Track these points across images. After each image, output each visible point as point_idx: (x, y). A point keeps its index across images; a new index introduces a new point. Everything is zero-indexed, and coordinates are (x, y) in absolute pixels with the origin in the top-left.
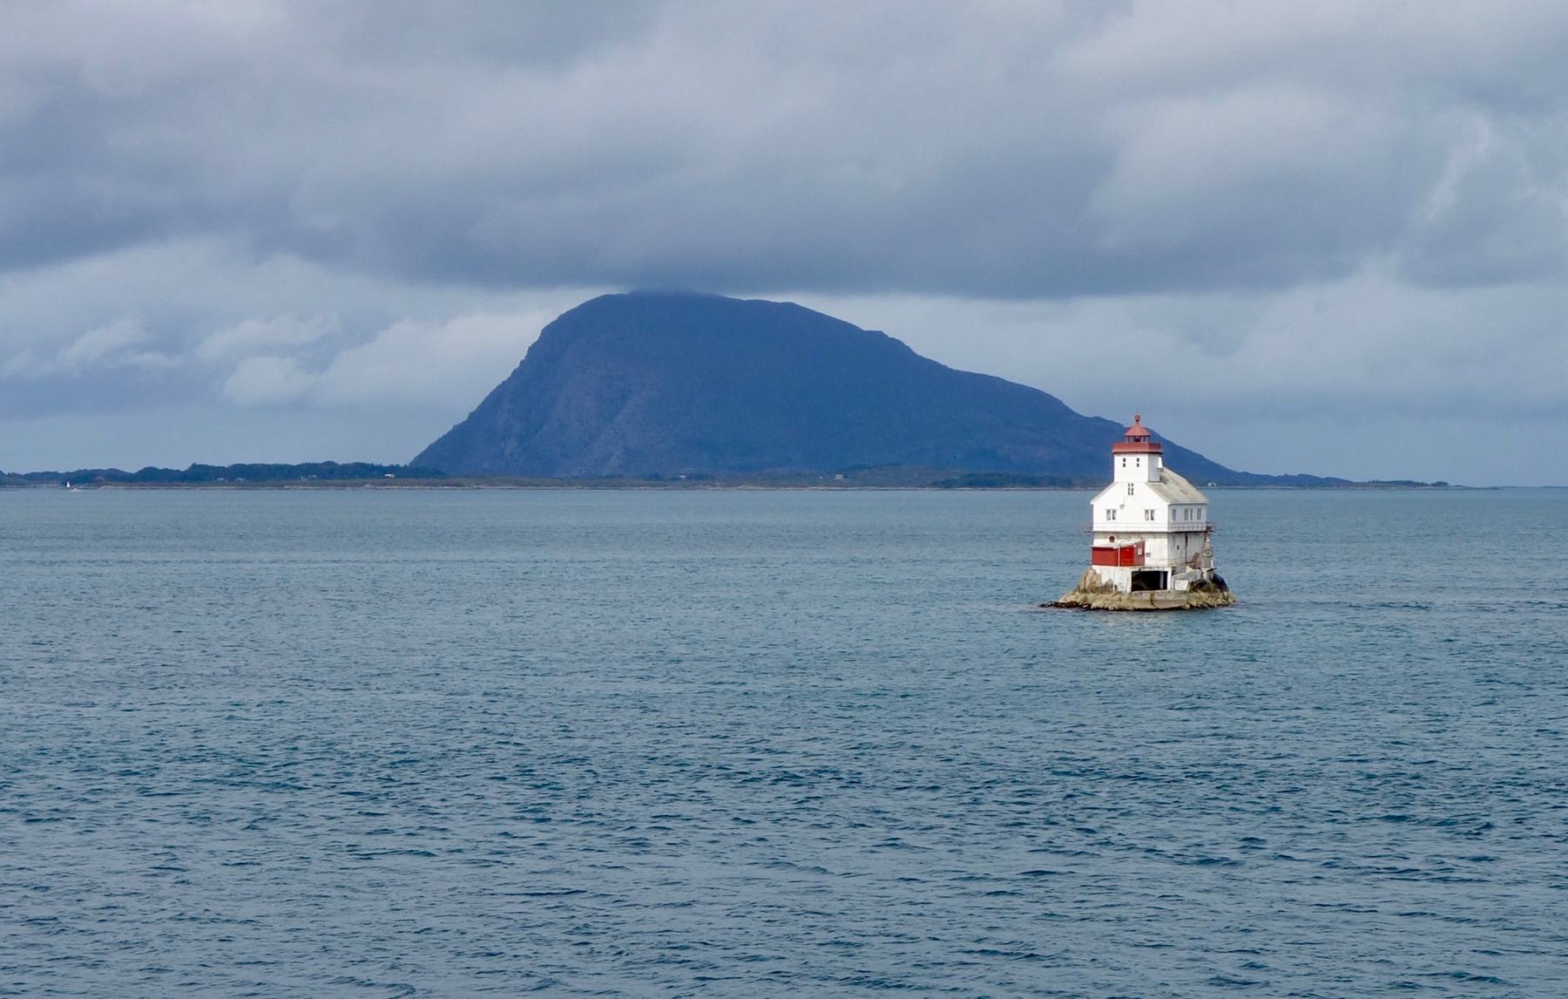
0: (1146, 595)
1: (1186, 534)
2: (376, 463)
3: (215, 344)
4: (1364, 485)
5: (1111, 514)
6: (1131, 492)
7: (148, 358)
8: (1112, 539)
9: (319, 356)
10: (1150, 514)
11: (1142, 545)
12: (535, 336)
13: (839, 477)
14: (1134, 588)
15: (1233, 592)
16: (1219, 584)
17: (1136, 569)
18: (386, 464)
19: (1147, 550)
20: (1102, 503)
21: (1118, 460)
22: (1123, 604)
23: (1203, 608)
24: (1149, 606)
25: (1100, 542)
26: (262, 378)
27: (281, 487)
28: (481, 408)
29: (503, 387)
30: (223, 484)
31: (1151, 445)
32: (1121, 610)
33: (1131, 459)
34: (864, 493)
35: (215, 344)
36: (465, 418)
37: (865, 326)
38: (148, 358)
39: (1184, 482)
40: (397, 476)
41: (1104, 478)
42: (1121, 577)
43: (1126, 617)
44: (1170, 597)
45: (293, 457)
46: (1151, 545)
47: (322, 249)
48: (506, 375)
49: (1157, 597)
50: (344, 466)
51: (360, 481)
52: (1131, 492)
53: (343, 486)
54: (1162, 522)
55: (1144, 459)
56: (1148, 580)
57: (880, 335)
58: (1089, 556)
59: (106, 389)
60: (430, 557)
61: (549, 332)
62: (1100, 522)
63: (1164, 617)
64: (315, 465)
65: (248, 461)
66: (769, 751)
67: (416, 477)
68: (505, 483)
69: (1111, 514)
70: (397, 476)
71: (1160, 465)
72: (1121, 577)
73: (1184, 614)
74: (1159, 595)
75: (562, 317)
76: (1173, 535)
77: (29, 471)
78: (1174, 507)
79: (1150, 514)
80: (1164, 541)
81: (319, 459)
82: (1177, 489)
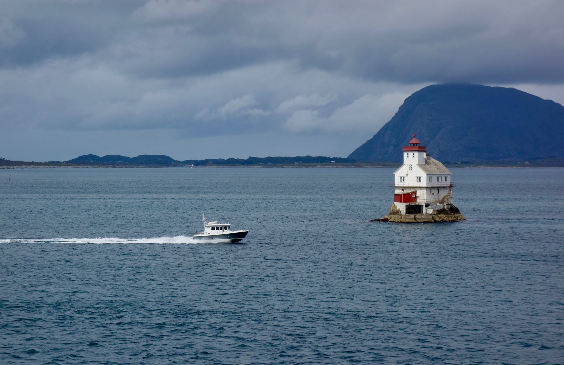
0: (412, 216)
1: (438, 188)
3: (284, 106)
4: (187, 163)
7: (255, 112)
8: (403, 190)
9: (327, 111)
10: (419, 179)
11: (415, 193)
12: (402, 103)
13: (527, 162)
14: (406, 213)
15: (463, 214)
16: (454, 210)
17: (408, 204)
18: (331, 157)
19: (417, 196)
20: (398, 174)
21: (405, 154)
22: (402, 220)
23: (443, 222)
24: (414, 221)
25: (398, 192)
26: (302, 120)
27: (282, 166)
28: (379, 133)
29: (388, 124)
30: (261, 165)
31: (419, 147)
32: (401, 222)
33: (411, 154)
35: (284, 106)
36: (372, 137)
37: (545, 98)
38: (255, 112)
39: (440, 164)
41: (399, 163)
42: (401, 207)
44: (424, 217)
45: (293, 154)
46: (419, 193)
47: (329, 65)
48: (389, 119)
49: (417, 217)
51: (316, 164)
53: (309, 166)
54: (424, 182)
55: (416, 154)
56: (417, 209)
57: (550, 102)
58: (393, 197)
59: (237, 125)
60: (168, 197)
61: (407, 101)
62: (398, 182)
63: (423, 227)
64: (301, 157)
65: (273, 156)
66: (338, 279)
68: (379, 165)
69: (402, 179)
71: (425, 156)
72: (401, 207)
73: (430, 224)
74: (418, 216)
75: (413, 94)
76: (429, 188)
78: (430, 176)
79: (419, 179)
81: (304, 155)
82: (434, 167)
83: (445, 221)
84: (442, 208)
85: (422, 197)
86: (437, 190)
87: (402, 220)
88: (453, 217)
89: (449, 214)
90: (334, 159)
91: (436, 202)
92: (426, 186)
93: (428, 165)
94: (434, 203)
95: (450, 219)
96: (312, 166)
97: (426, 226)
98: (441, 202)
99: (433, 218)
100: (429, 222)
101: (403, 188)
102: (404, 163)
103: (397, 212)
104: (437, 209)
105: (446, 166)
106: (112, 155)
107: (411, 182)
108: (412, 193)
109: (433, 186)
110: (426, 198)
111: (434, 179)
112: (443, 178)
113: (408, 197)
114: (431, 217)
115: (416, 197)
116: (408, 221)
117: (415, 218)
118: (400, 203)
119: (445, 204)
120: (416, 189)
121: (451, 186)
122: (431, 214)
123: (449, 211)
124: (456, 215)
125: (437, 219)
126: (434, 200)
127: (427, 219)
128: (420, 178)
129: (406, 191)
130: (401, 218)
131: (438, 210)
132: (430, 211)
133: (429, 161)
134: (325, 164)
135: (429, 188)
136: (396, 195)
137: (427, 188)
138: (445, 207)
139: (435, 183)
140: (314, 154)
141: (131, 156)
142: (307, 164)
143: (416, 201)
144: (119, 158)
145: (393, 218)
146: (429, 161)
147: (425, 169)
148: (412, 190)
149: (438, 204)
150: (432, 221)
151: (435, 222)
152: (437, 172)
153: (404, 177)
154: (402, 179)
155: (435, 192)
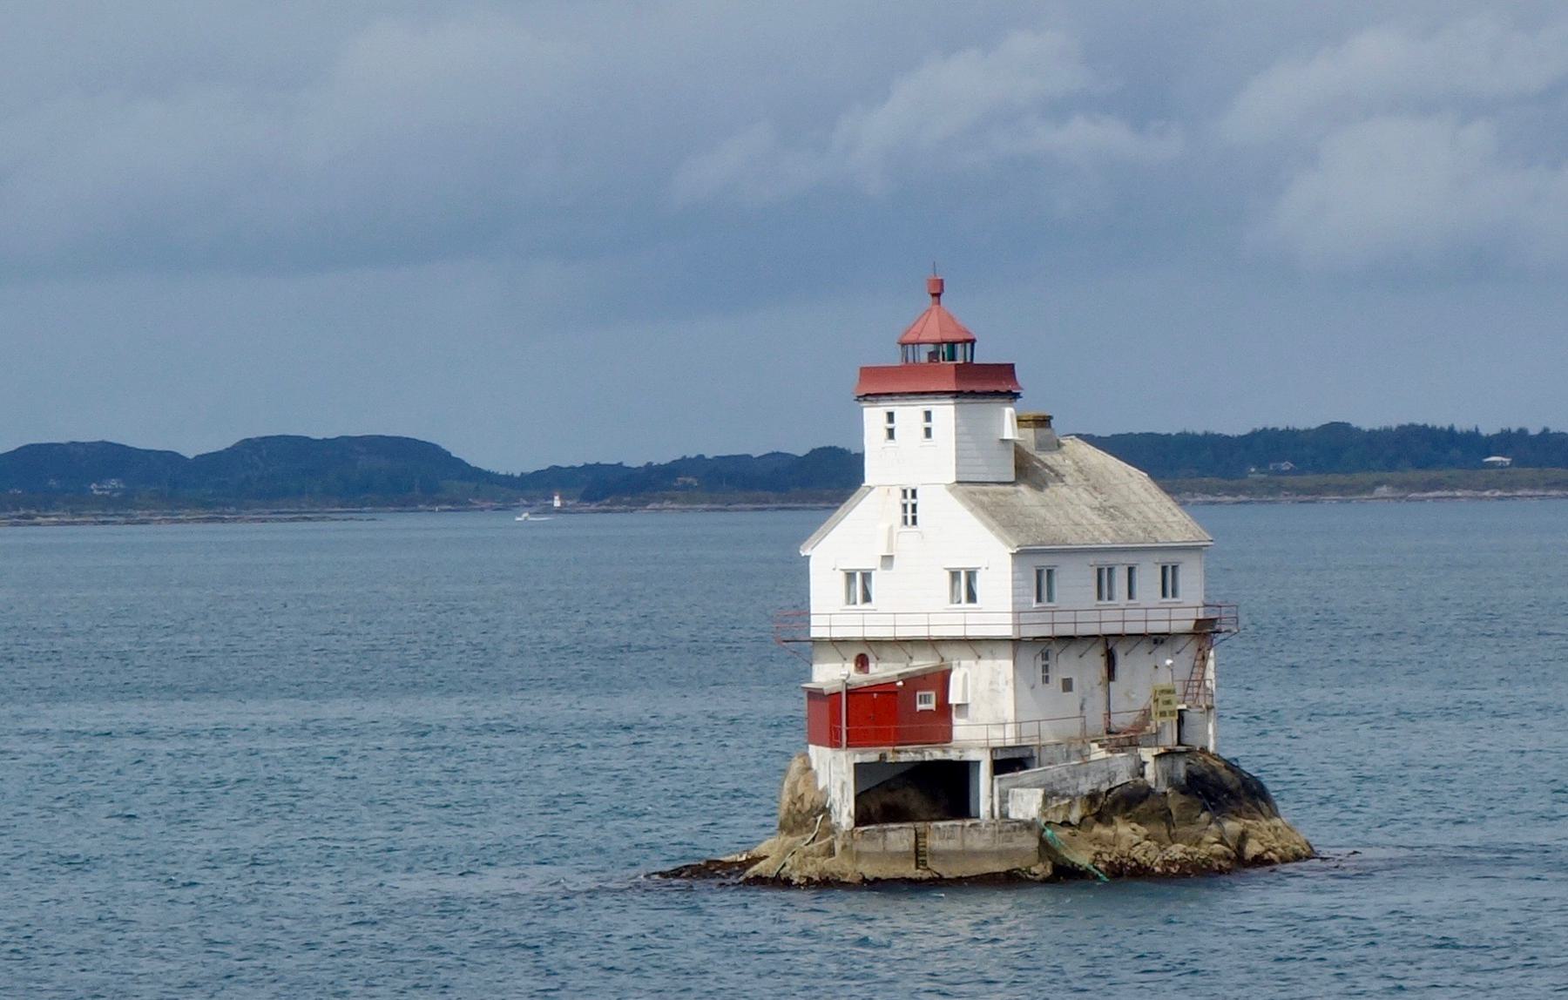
0: (899, 837)
1: (1110, 647)
2: (1463, 425)
5: (859, 584)
6: (911, 515)
8: (862, 662)
10: (965, 584)
11: (940, 680)
14: (862, 818)
15: (1292, 821)
16: (1219, 789)
17: (871, 756)
18: (1489, 429)
19: (954, 698)
20: (836, 547)
22: (838, 865)
24: (911, 871)
27: (972, 510)
33: (909, 414)
34: (769, 517)
40: (1519, 462)
42: (834, 773)
43: (837, 905)
44: (977, 842)
49: (934, 843)
50: (1372, 432)
52: (911, 515)
53: (1318, 491)
54: (996, 610)
55: (945, 413)
56: (947, 788)
62: (830, 613)
67: (1422, 464)
70: (1519, 462)
71: (1009, 431)
74: (944, 836)
76: (1038, 650)
77: (676, 455)
78: (1040, 568)
79: (965, 584)
80: (1003, 666)
81: (1306, 417)
83: (1141, 872)
84: (1123, 777)
85: (987, 708)
86: (1094, 662)
87: (831, 866)
88: (1211, 837)
89: (1198, 818)
90: (1508, 441)
91: (1086, 739)
92: (1008, 631)
93: (1039, 486)
94: (1075, 748)
95: (1177, 851)
96: (1341, 489)
97: (998, 904)
98: (1124, 740)
99: (1045, 848)
100: (1010, 880)
101: (863, 651)
102: (868, 481)
103: (808, 816)
104: (1086, 787)
105: (1169, 491)
106: (422, 438)
107: (912, 605)
108: (915, 682)
109: (1068, 630)
110: (1009, 714)
111: (1075, 585)
112: (1148, 579)
113: (890, 713)
114: (1030, 843)
115: (944, 709)
116: (870, 870)
117: (919, 855)
118: (827, 752)
119: (1147, 754)
120: (949, 653)
121: (1204, 631)
122: (1028, 826)
123: (1175, 802)
124: (1233, 826)
125: (1082, 857)
126: (1074, 728)
127: (1000, 855)
128: (971, 575)
129: (882, 671)
130: (830, 852)
131: (1093, 797)
132: (1027, 803)
133: (1049, 458)
134: (1342, 479)
135: (1038, 650)
136: (815, 695)
137: (1016, 643)
138: (1150, 773)
139: (1079, 606)
140: (1373, 412)
141: (191, 446)
142: (1310, 479)
143: (946, 737)
144: (112, 460)
145: (774, 852)
146: (1049, 458)
147: (1003, 518)
148: (922, 662)
149: (1097, 753)
150: (1042, 869)
151: (1065, 874)
152: (1102, 532)
153: (866, 576)
154: (859, 584)
155: (1087, 669)
